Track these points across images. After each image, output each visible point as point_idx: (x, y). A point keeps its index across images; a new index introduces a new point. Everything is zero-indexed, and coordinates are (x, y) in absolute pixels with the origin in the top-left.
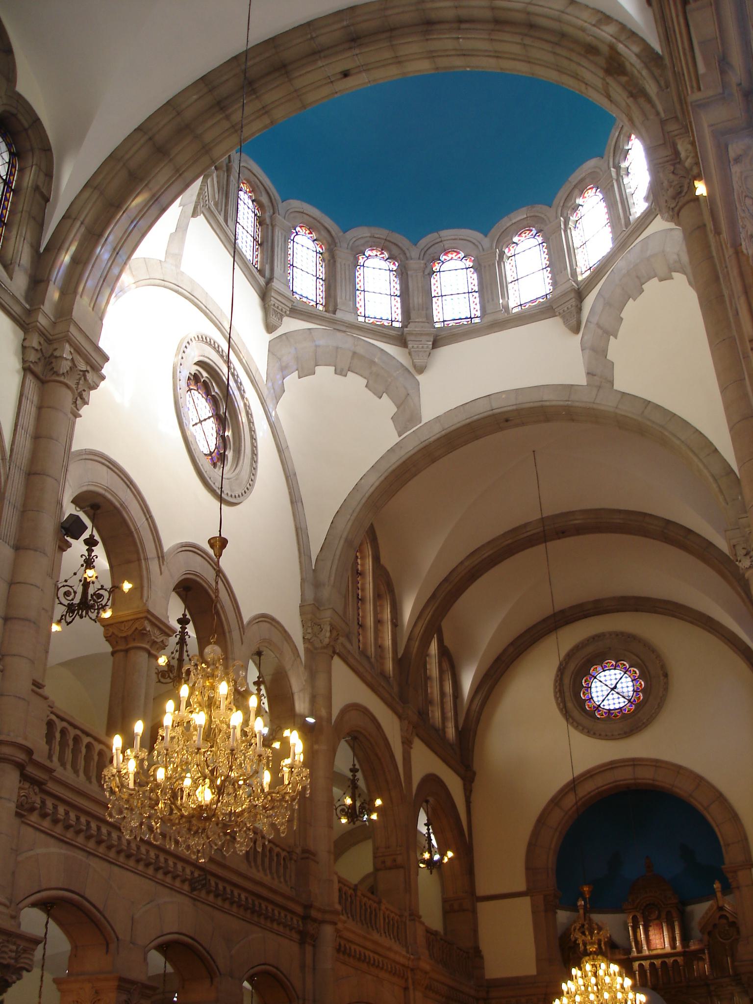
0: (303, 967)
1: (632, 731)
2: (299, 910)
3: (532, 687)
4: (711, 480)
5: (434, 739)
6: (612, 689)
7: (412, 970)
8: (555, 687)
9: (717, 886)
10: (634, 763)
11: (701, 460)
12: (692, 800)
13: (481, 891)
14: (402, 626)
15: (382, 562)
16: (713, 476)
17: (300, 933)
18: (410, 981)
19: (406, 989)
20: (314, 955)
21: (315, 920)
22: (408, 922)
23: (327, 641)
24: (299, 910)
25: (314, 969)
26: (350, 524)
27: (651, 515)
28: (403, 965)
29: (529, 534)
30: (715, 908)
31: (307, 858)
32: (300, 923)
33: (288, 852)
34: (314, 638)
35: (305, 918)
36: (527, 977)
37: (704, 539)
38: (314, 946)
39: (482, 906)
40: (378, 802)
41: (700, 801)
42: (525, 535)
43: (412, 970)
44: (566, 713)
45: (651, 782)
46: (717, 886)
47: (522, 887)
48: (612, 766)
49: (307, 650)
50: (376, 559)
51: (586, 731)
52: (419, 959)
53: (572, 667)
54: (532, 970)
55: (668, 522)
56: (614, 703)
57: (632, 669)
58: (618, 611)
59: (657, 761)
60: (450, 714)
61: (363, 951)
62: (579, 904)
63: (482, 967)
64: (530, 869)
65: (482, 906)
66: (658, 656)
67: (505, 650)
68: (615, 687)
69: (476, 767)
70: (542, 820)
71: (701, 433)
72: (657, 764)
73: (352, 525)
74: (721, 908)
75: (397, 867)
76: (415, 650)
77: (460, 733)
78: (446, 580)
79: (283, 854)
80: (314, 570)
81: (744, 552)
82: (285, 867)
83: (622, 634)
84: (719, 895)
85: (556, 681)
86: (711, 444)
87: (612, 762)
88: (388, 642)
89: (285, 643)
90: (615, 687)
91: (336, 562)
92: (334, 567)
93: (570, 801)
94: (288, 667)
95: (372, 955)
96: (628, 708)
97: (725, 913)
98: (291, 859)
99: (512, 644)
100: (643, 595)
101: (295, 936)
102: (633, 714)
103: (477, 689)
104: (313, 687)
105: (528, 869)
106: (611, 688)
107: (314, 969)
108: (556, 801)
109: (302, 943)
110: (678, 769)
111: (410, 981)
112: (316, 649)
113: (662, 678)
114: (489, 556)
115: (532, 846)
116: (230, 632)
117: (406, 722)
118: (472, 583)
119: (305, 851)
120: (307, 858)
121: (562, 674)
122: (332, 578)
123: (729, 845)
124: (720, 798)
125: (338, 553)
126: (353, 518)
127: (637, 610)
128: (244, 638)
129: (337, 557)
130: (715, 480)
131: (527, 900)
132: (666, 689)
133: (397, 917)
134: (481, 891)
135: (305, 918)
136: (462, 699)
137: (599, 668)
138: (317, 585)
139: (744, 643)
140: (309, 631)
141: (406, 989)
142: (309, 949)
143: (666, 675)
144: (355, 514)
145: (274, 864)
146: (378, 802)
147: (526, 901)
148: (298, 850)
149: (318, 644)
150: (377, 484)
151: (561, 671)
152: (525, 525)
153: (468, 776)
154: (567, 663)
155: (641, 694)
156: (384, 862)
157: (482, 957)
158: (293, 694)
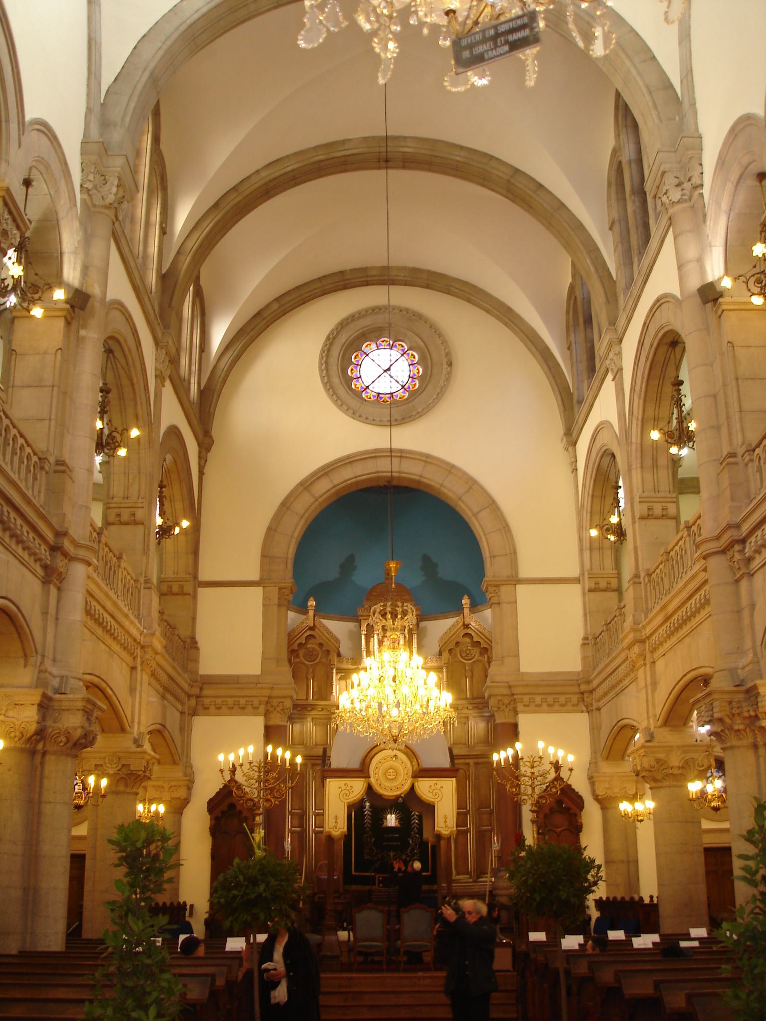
0: (45, 613)
1: (403, 419)
2: (49, 535)
3: (293, 354)
4: (645, 90)
5: (180, 388)
6: (385, 371)
7: (143, 647)
8: (321, 357)
9: (466, 601)
10: (402, 455)
11: (635, 66)
12: (460, 503)
13: (203, 576)
14: (172, 234)
15: (162, 146)
16: (647, 86)
17: (45, 567)
18: (139, 661)
19: (133, 668)
20: (58, 601)
21: (65, 555)
22: (142, 591)
23: (111, 198)
24: (49, 535)
25: (57, 619)
26: (161, 53)
27: (497, 159)
28: (135, 640)
29: (347, 153)
30: (461, 624)
31: (64, 472)
32: (48, 553)
33: (40, 459)
34: (95, 191)
35: (55, 549)
36: (248, 676)
37: (556, 198)
38: (59, 589)
39: (202, 592)
40: (135, 433)
41: (468, 507)
42: (342, 154)
43: (143, 647)
44: (329, 386)
45: (418, 478)
46: (466, 601)
47: (255, 576)
48: (374, 455)
49: (83, 201)
50: (156, 140)
51: (351, 411)
52: (153, 634)
53: (343, 338)
54: (257, 671)
55: (517, 171)
56: (384, 386)
57: (410, 352)
58: (406, 284)
59: (428, 456)
60: (195, 368)
61: (102, 611)
62: (309, 604)
63: (196, 661)
64: (266, 557)
65: (202, 592)
66: (444, 342)
67: (268, 306)
68: (389, 369)
69: (214, 433)
70: (286, 505)
71: (637, 34)
72: (427, 459)
73: (161, 59)
74: (466, 626)
75: (136, 523)
76: (185, 267)
77: (202, 393)
78: (234, 189)
79: (35, 459)
80: (102, 105)
81: (676, 181)
82: (35, 479)
83: (407, 310)
84: (466, 611)
85: (323, 351)
86: (649, 50)
87: (376, 451)
88: (153, 249)
89: (63, 179)
90: (389, 369)
91: (135, 98)
92: (132, 105)
93: (324, 487)
94: (61, 214)
95: (109, 619)
96: (400, 394)
97: (469, 631)
98: (42, 468)
99: (277, 299)
100: (439, 271)
101: (40, 571)
102: (404, 402)
103: (227, 347)
104: (87, 254)
105: (263, 556)
106: (384, 369)
107: (57, 619)
108: (306, 485)
109: (46, 582)
110: (450, 469)
111: (139, 661)
112: (94, 206)
113: (445, 366)
114: (293, 171)
115: (271, 531)
116: (7, 121)
117: (164, 351)
118: (264, 202)
119: (60, 463)
120: (64, 472)
121: (331, 344)
122: (128, 119)
123: (494, 557)
124: (492, 505)
125: (140, 87)
126: (165, 47)
127: (427, 287)
128: (23, 138)
129: (137, 92)
130: (650, 92)
131: (259, 590)
132: (448, 379)
133: (132, 582)
134: (203, 576)
135: (55, 549)
136: (209, 353)
137: (374, 346)
138: (105, 124)
139: (542, 341)
140: (91, 177)
141: (133, 668)
142: (53, 591)
143: (450, 364)
144: (169, 43)
145: (24, 467)
146: (135, 433)
147: (257, 593)
148: (52, 460)
149: (98, 201)
150: (205, 10)
151: (331, 340)
152: (344, 142)
153: (206, 443)
154: (338, 333)
155: (417, 382)
156: (119, 515)
157: (197, 649)
158: (61, 254)
